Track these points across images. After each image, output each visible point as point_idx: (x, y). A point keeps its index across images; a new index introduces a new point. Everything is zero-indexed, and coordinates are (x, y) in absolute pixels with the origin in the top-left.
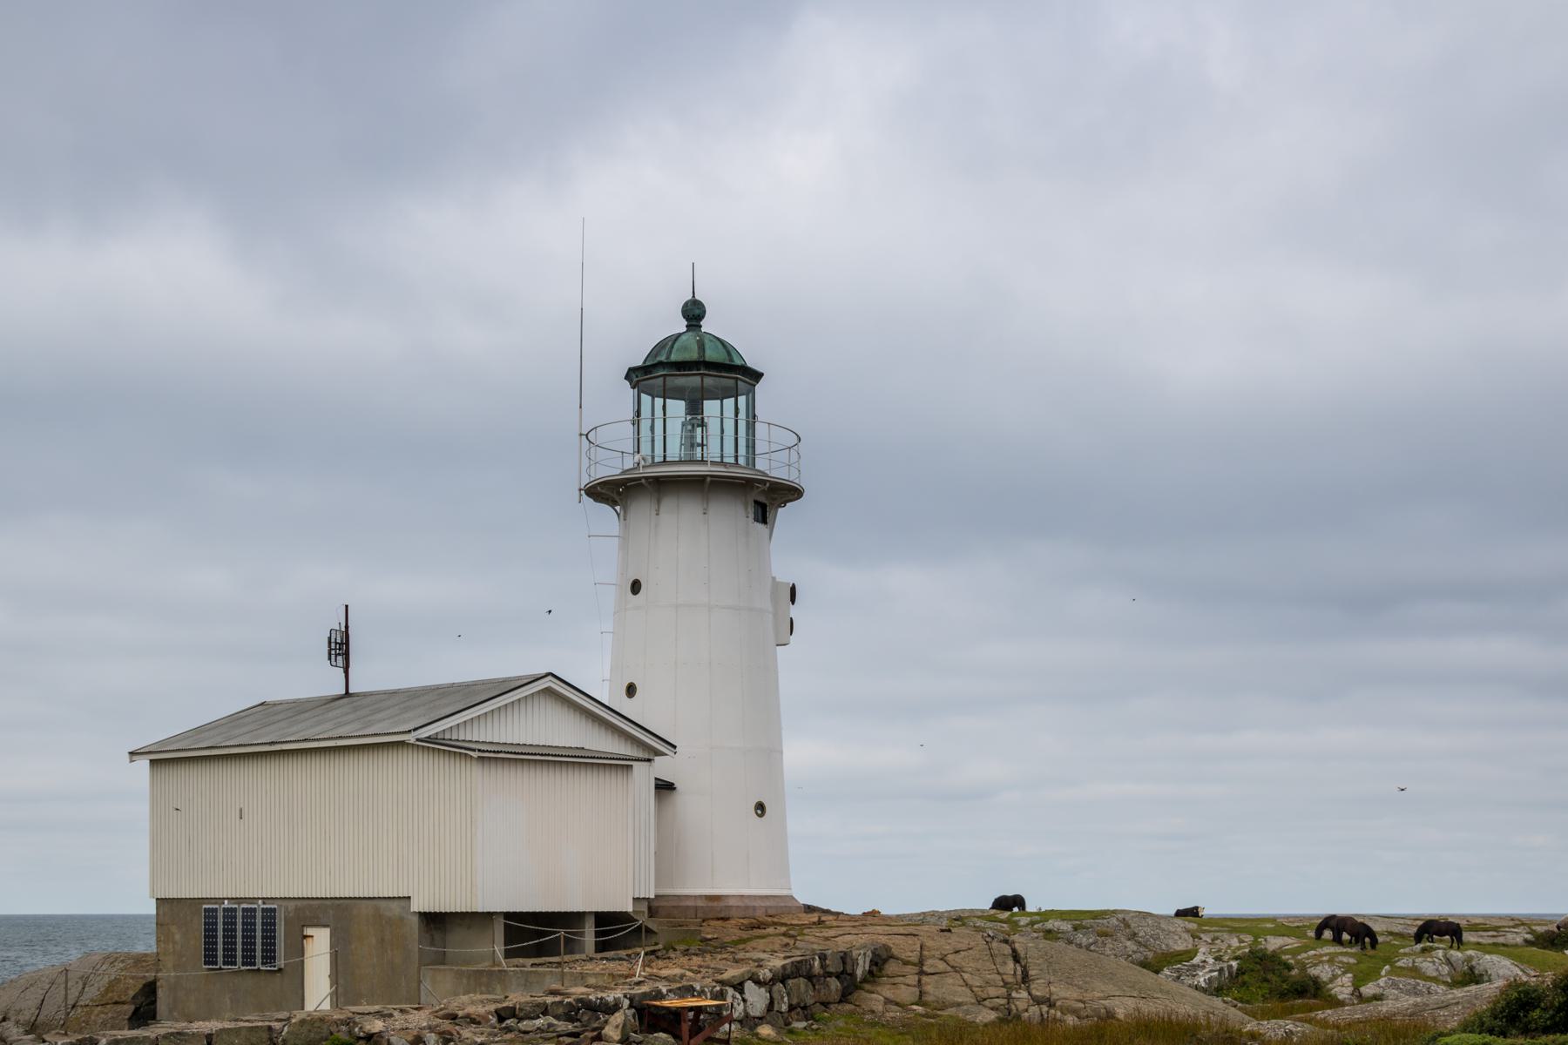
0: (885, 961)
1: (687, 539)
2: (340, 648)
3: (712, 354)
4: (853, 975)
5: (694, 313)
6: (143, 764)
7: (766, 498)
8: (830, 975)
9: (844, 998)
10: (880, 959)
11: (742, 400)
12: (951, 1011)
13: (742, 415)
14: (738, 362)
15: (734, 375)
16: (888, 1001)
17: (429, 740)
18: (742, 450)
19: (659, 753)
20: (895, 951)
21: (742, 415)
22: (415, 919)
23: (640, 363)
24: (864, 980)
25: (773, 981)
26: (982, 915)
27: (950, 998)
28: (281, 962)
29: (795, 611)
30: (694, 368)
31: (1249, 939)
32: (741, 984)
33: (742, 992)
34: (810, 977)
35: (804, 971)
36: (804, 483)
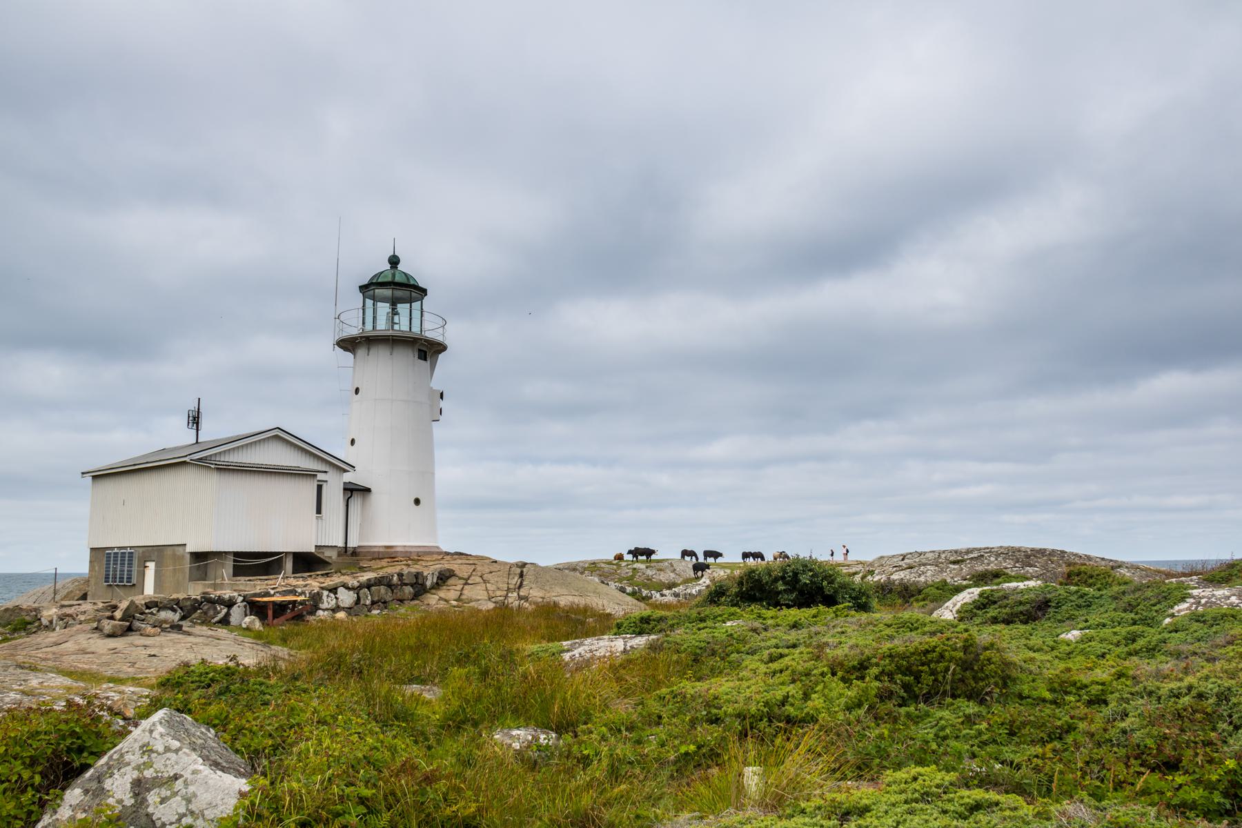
0: (448, 578)
1: (383, 370)
3: (397, 279)
4: (423, 585)
5: (394, 261)
6: (89, 479)
8: (406, 585)
9: (416, 596)
10: (444, 578)
12: (472, 604)
16: (441, 599)
17: (200, 460)
18: (369, 312)
19: (345, 471)
20: (457, 572)
22: (188, 556)
24: (432, 588)
25: (361, 587)
26: (610, 563)
27: (475, 597)
28: (134, 581)
29: (442, 404)
30: (395, 286)
31: (728, 571)
32: (336, 589)
33: (336, 593)
34: (390, 586)
35: (385, 582)
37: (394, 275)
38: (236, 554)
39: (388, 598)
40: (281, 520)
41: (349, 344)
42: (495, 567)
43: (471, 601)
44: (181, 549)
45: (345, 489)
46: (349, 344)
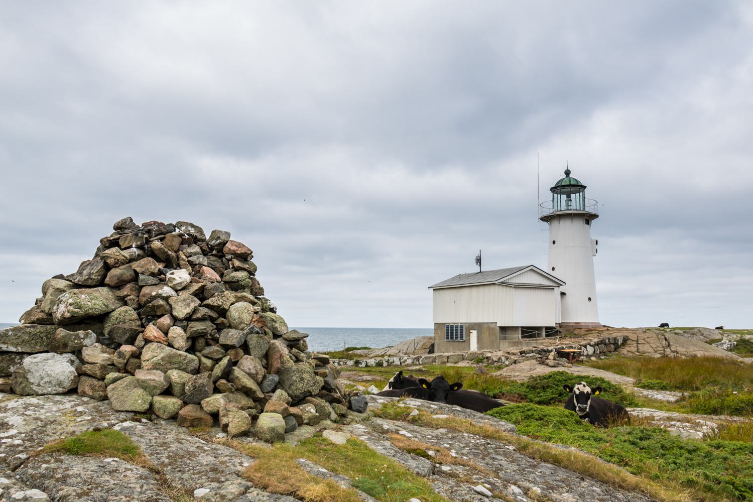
1: (568, 230)
2: (479, 261)
4: (618, 344)
5: (568, 173)
6: (432, 289)
7: (588, 218)
8: (611, 344)
9: (615, 350)
10: (625, 340)
11: (581, 193)
12: (647, 354)
13: (581, 197)
14: (580, 184)
15: (579, 187)
16: (628, 351)
17: (501, 283)
19: (561, 285)
20: (630, 337)
21: (581, 197)
22: (498, 328)
23: (554, 186)
24: (621, 345)
29: (597, 247)
30: (568, 187)
31: (739, 335)
33: (586, 348)
34: (605, 344)
35: (603, 343)
36: (599, 214)
37: (570, 181)
38: (522, 327)
39: (605, 351)
40: (540, 311)
41: (547, 219)
42: (648, 334)
43: (645, 353)
44: (493, 325)
45: (561, 294)
46: (547, 219)
